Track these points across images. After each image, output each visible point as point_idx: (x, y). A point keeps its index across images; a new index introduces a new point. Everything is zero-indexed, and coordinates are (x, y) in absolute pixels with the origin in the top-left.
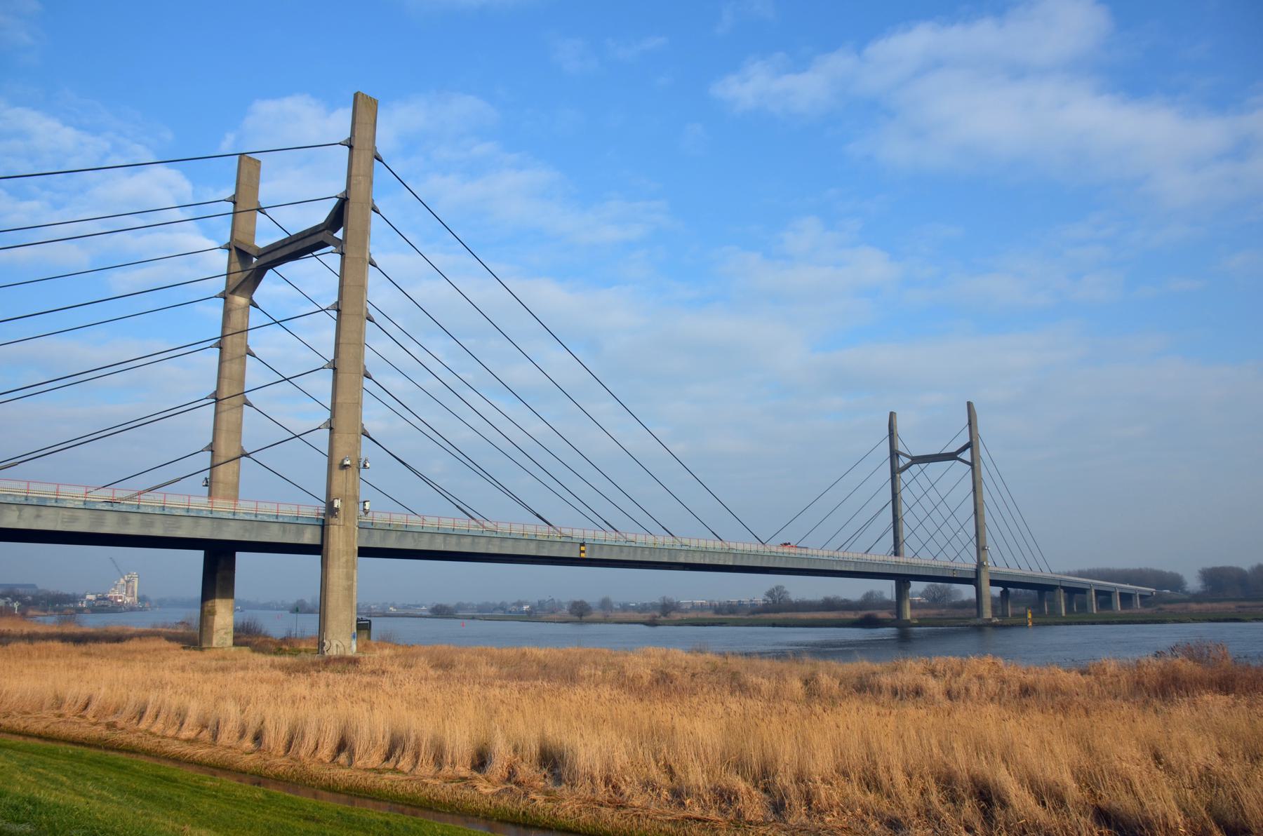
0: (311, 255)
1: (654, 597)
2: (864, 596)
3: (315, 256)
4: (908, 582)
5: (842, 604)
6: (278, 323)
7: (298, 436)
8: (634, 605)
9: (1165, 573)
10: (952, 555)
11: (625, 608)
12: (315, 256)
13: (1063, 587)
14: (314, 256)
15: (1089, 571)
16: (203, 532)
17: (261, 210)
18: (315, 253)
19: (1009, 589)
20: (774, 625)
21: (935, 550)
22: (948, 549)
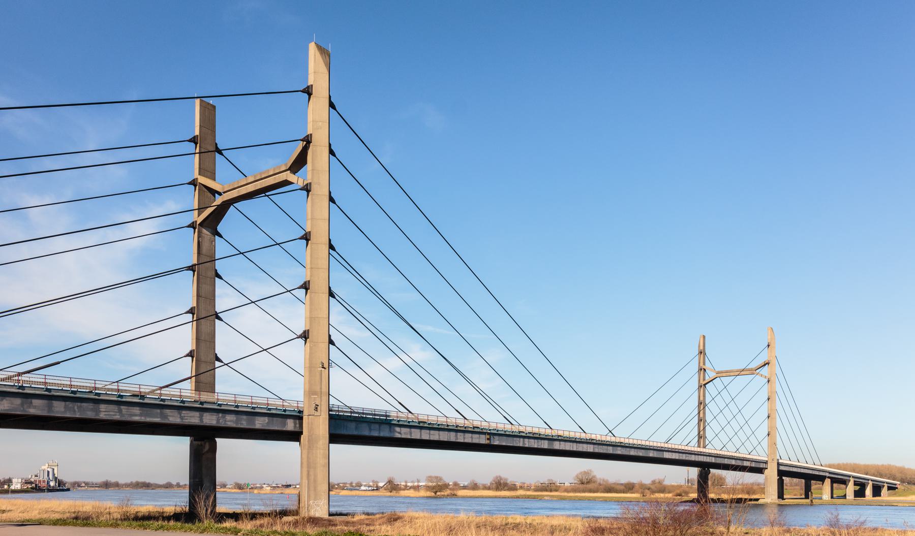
0: (264, 195)
1: (544, 479)
2: (908, 469)
3: (268, 196)
4: (708, 469)
5: (612, 485)
6: (242, 253)
7: (265, 350)
8: (462, 485)
9: (912, 470)
10: (750, 449)
11: (96, 484)
12: (268, 196)
13: (481, 489)
14: (266, 196)
15: (839, 464)
16: (193, 419)
17: (220, 152)
18: (267, 194)
19: (784, 478)
20: (727, 372)
21: (738, 444)
22: (747, 444)
